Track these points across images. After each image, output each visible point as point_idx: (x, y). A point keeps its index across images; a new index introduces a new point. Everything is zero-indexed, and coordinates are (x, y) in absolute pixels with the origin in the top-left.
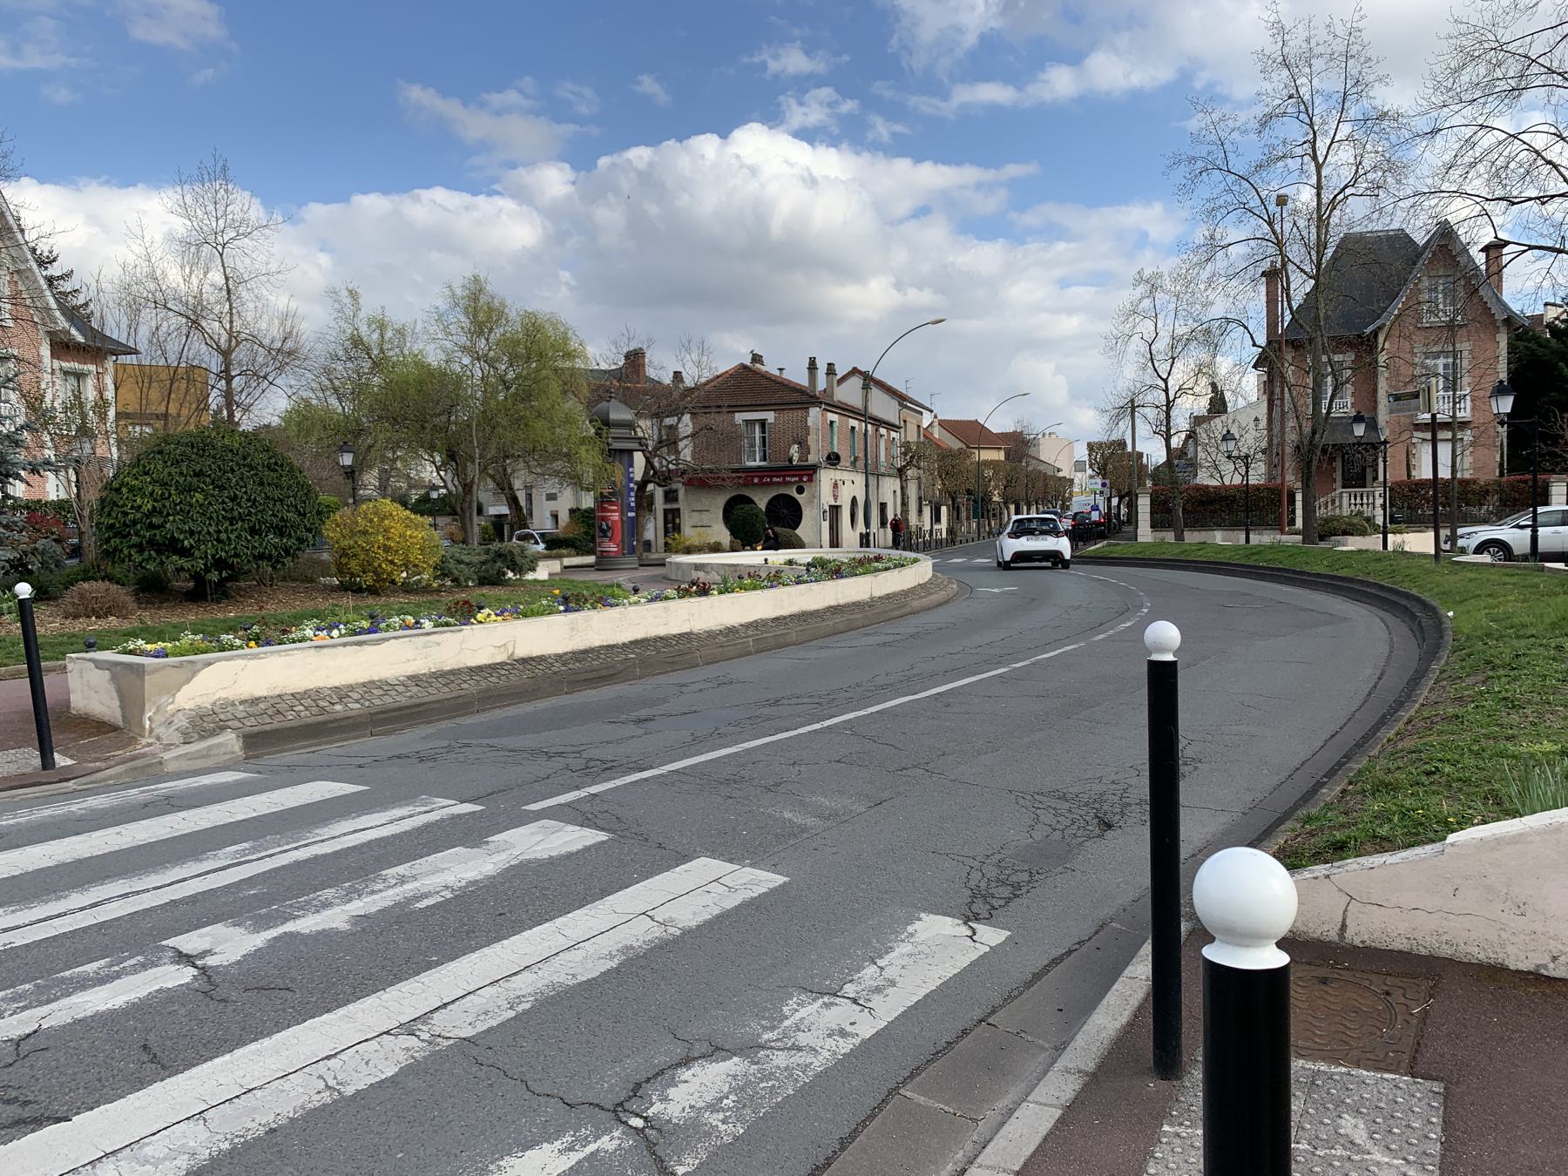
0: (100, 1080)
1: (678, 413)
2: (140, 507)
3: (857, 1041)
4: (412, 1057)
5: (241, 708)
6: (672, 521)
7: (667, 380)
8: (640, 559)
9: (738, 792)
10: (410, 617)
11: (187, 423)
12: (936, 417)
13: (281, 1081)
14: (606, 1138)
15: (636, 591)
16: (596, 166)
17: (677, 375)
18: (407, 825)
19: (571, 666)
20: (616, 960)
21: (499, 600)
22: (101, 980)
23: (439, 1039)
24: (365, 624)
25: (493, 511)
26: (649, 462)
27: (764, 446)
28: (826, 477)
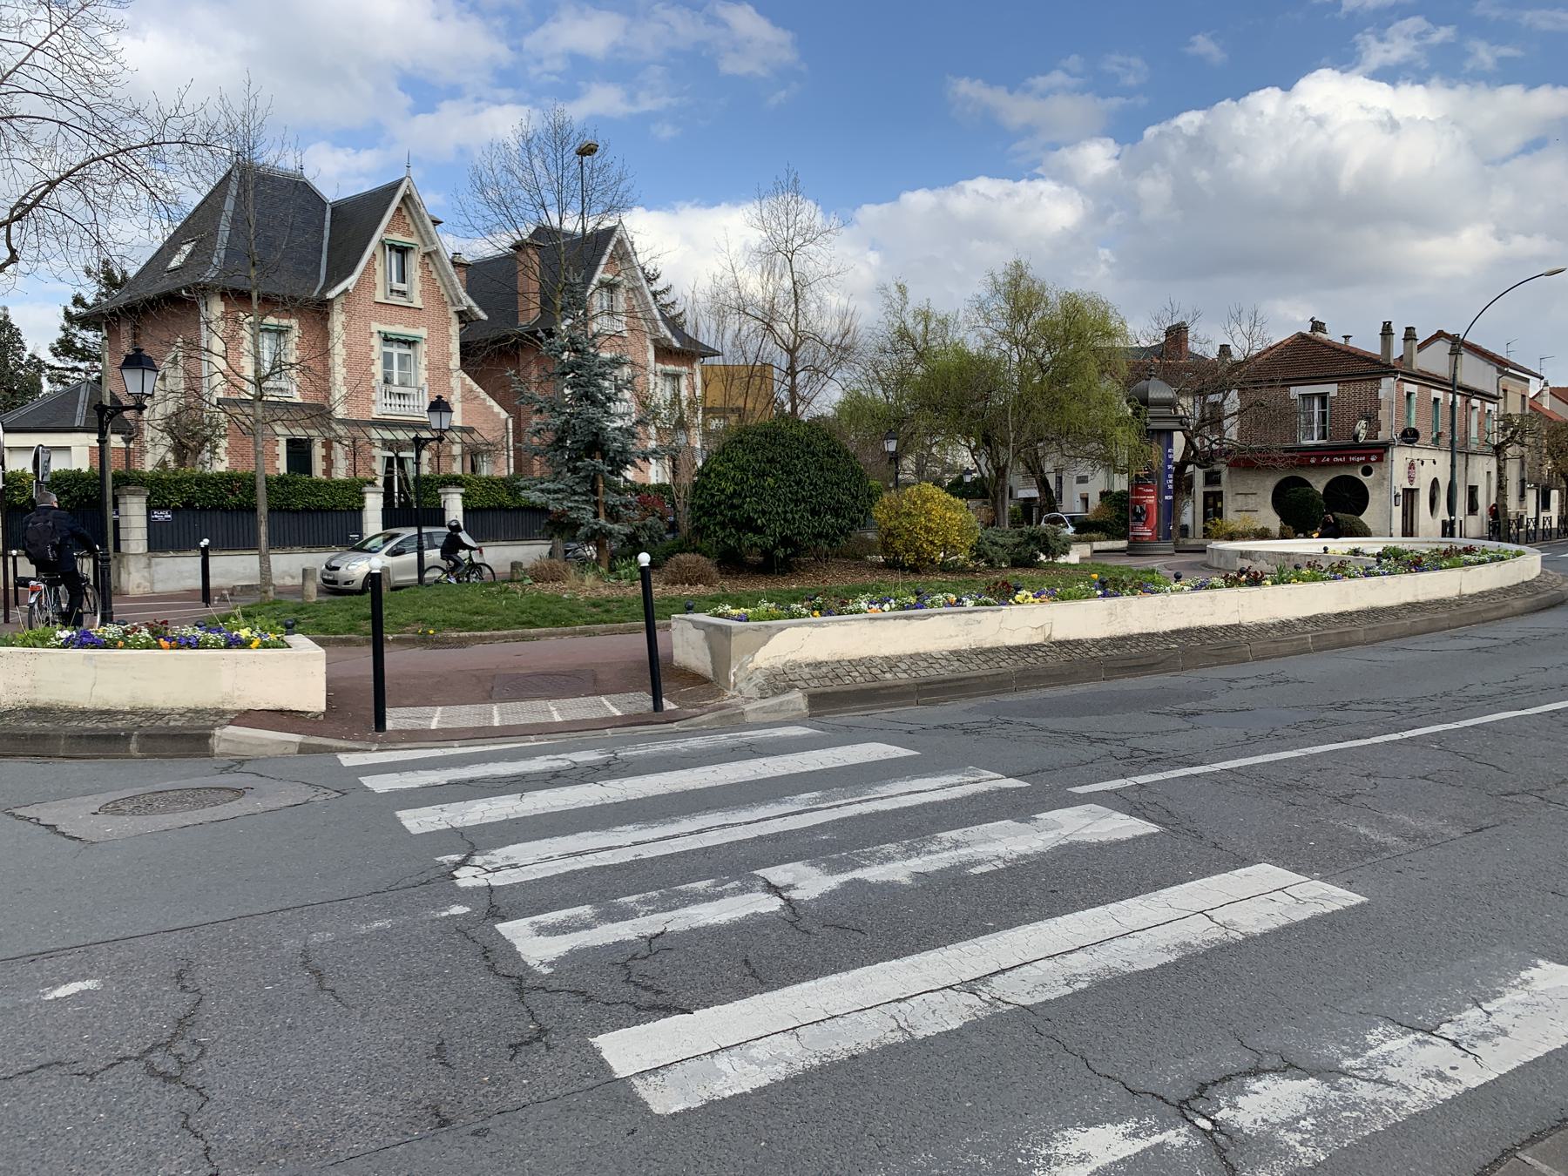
0: (712, 983)
1: (1224, 388)
2: (724, 490)
3: (1461, 1089)
4: (975, 1015)
5: (807, 670)
6: (1213, 506)
7: (1213, 354)
8: (1176, 544)
9: (1303, 800)
10: (952, 596)
11: (760, 416)
12: (1546, 384)
13: (860, 1014)
14: (1172, 1133)
15: (1178, 578)
16: (1142, 137)
17: (1224, 350)
18: (957, 793)
19: (1109, 652)
20: (1173, 955)
21: (1032, 582)
22: (709, 897)
23: (999, 1003)
24: (913, 600)
25: (1022, 494)
26: (1189, 441)
27: (1324, 422)
28: (1400, 457)
